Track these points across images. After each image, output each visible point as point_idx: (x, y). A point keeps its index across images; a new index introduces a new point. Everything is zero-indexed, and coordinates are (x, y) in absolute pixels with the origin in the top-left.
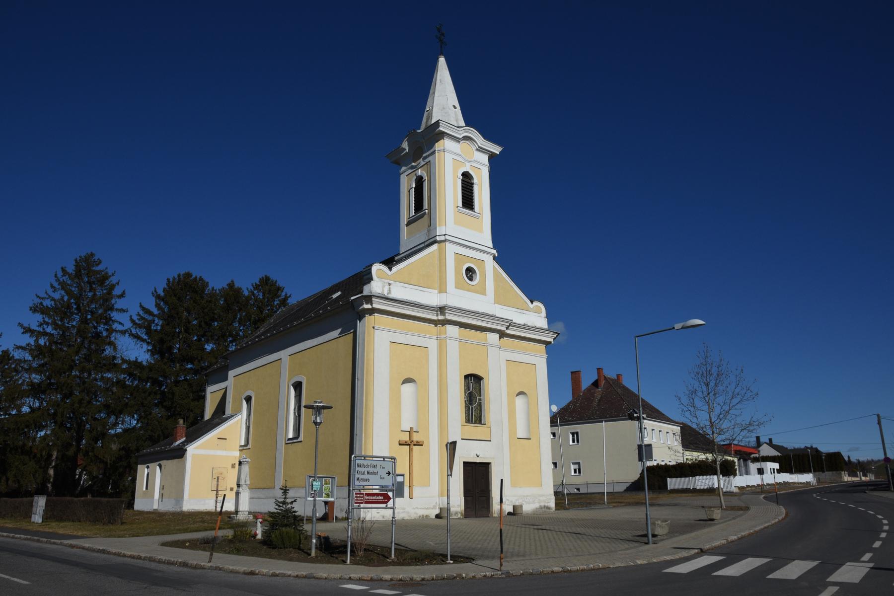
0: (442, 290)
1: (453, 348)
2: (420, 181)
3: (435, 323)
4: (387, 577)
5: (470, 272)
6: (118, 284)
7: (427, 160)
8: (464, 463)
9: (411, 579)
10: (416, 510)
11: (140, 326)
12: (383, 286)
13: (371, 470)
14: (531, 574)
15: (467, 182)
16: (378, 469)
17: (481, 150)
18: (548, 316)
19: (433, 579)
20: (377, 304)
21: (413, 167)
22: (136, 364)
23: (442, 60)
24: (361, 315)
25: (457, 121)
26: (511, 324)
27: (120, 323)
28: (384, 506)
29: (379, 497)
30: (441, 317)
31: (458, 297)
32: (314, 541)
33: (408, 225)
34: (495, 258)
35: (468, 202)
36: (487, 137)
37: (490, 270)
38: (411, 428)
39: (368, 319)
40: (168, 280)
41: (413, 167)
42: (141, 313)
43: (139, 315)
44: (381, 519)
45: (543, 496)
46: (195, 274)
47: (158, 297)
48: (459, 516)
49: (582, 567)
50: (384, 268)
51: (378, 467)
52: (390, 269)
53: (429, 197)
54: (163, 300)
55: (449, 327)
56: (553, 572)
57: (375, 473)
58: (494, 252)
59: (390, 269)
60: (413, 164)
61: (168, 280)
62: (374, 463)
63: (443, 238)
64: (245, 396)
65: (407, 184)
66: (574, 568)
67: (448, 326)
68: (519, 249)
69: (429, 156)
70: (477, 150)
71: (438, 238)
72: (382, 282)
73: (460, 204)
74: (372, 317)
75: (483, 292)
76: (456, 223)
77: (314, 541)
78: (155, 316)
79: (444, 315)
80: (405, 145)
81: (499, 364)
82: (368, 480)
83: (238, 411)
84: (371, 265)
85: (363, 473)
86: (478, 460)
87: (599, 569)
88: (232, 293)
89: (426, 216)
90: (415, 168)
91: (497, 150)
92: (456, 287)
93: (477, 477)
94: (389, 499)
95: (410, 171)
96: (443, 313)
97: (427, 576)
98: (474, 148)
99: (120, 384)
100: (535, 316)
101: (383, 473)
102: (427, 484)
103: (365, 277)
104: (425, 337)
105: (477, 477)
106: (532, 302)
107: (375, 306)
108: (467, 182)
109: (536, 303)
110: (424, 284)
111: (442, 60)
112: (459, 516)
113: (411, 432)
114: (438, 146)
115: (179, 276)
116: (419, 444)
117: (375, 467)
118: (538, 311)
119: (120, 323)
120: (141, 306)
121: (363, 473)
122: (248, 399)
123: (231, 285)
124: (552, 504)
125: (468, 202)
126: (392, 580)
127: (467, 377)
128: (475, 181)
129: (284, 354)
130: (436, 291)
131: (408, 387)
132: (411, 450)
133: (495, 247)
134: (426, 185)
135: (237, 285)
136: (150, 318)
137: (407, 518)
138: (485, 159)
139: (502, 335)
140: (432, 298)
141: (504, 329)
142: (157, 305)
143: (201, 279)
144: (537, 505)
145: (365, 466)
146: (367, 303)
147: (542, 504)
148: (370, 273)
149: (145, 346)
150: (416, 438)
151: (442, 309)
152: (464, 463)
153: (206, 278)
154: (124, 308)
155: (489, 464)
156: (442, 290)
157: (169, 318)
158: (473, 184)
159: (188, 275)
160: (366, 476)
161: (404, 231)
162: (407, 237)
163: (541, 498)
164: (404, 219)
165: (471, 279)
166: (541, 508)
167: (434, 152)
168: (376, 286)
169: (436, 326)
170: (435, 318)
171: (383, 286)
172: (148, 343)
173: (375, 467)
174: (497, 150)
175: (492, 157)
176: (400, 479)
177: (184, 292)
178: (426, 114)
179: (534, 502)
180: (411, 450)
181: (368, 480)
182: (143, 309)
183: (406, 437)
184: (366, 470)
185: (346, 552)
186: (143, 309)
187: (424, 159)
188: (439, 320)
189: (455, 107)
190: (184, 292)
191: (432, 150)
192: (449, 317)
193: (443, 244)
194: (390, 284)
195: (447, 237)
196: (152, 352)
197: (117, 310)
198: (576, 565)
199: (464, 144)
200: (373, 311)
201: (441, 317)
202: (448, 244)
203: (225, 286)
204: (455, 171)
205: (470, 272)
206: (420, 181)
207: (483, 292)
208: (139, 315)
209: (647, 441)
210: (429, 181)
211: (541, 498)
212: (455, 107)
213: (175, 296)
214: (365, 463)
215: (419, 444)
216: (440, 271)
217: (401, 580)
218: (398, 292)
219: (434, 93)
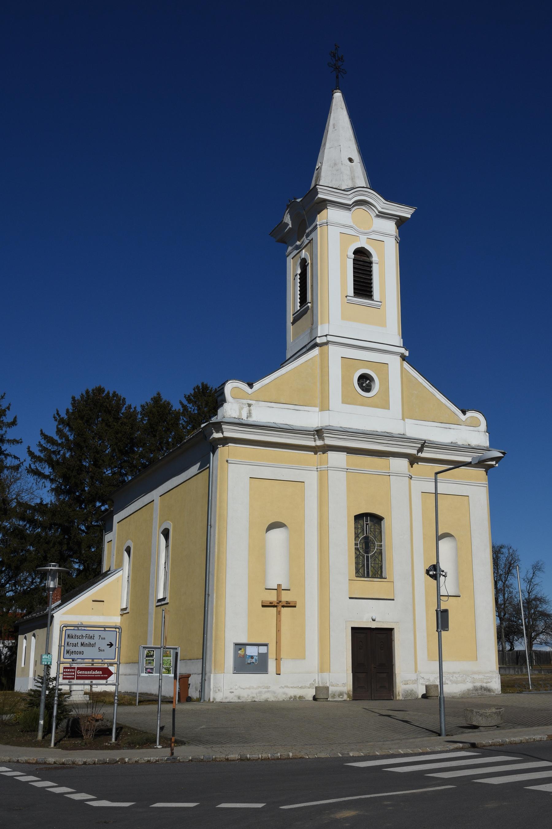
0: (324, 407)
1: (338, 482)
2: (304, 264)
3: (315, 450)
4: (23, 759)
5: (365, 382)
6: (8, 408)
7: (309, 238)
8: (353, 629)
9: (73, 763)
10: (286, 690)
11: (39, 459)
12: (241, 409)
13: (86, 641)
14: (202, 761)
15: (362, 262)
16: (96, 640)
17: (382, 215)
18: (489, 430)
19: (94, 763)
20: (229, 432)
21: (297, 247)
22: (41, 508)
23: (338, 96)
24: (214, 446)
25: (353, 179)
26: (424, 445)
27: (16, 457)
28: (104, 682)
29: (97, 672)
30: (319, 442)
31: (347, 415)
32: (42, 722)
33: (293, 323)
34: (403, 358)
35: (363, 287)
36: (388, 197)
37: (396, 374)
38: (279, 586)
39: (221, 450)
40: (73, 398)
41: (297, 247)
42: (43, 442)
43: (40, 445)
44: (236, 700)
45: (479, 673)
46: (109, 388)
47: (61, 421)
48: (345, 697)
49: (264, 756)
50: (244, 386)
51: (97, 637)
52: (251, 385)
53: (312, 286)
54: (68, 425)
55: (331, 455)
56: (227, 760)
57: (90, 645)
58: (403, 350)
59: (251, 385)
60: (298, 243)
61: (73, 398)
62: (91, 634)
63: (324, 340)
64: (125, 548)
65: (293, 269)
66: (255, 756)
67: (330, 453)
68: (434, 343)
69: (311, 232)
70: (377, 216)
71: (318, 340)
72: (239, 403)
73: (351, 291)
74: (226, 448)
75: (385, 405)
76: (344, 317)
77: (42, 722)
78: (58, 445)
79: (323, 440)
80: (287, 219)
81: (404, 500)
82: (82, 653)
83: (120, 566)
84: (224, 384)
85: (76, 645)
86: (374, 625)
87: (288, 758)
88: (159, 410)
89: (309, 312)
90: (299, 248)
91: (406, 212)
92: (343, 402)
93: (373, 650)
94: (110, 674)
95: (296, 252)
96: (321, 438)
97: (89, 760)
98: (373, 215)
99: (18, 533)
100: (471, 432)
101: (103, 644)
102: (300, 654)
103: (216, 400)
104: (304, 470)
105: (373, 650)
106: (464, 412)
107: (227, 434)
108: (362, 262)
109: (469, 414)
110: (300, 400)
111: (338, 96)
112: (345, 697)
113: (279, 589)
114: (320, 218)
115: (87, 392)
116: (289, 605)
117: (91, 638)
118: (475, 424)
119: (16, 457)
120: (42, 433)
121: (76, 645)
122: (128, 550)
123: (157, 400)
124: (496, 684)
125: (363, 287)
126: (55, 763)
127: (358, 518)
128: (375, 259)
129: (155, 494)
130: (317, 409)
131: (276, 533)
132: (279, 613)
133: (406, 345)
134: (309, 269)
135: (165, 398)
136: (55, 448)
137: (272, 698)
138: (391, 227)
139: (413, 460)
140: (310, 418)
141: (414, 452)
142: (59, 432)
143: (115, 394)
144: (469, 686)
145: (78, 637)
146: (217, 432)
147: (478, 684)
148: (223, 393)
149: (48, 484)
150: (285, 597)
151: (319, 433)
152: (353, 629)
153: (122, 393)
154: (18, 439)
155: (391, 630)
156: (324, 407)
157: (78, 446)
158: (371, 263)
159: (100, 390)
160: (79, 648)
161: (290, 329)
162: (293, 336)
163: (476, 676)
164: (290, 318)
165: (367, 389)
166: (476, 689)
167: (315, 228)
168: (230, 410)
169: (316, 453)
170: (312, 444)
171: (241, 409)
172: (52, 481)
173: (91, 638)
174: (406, 212)
175: (401, 222)
176: (263, 650)
177: (95, 412)
178: (316, 172)
179: (464, 682)
180: (279, 613)
181: (82, 653)
182: (45, 437)
183: (272, 597)
184: (79, 641)
185: (111, 734)
186: (45, 437)
187: (307, 237)
188: (317, 446)
189: (351, 160)
190: (95, 412)
191: (314, 225)
192: (329, 441)
193: (325, 347)
194: (250, 405)
195: (330, 338)
196: (57, 491)
197: (9, 441)
198: (323, 755)
199: (359, 211)
200: (225, 441)
201: (319, 443)
202: (331, 347)
203: (149, 400)
204: (343, 250)
205: (365, 382)
206: (304, 264)
207: (385, 405)
208: (40, 445)
209: (443, 607)
210: (312, 264)
211: (476, 676)
212: (351, 160)
213: (82, 418)
214: (79, 633)
215: (289, 605)
216: (322, 383)
217: (63, 764)
218: (263, 414)
219: (325, 144)
